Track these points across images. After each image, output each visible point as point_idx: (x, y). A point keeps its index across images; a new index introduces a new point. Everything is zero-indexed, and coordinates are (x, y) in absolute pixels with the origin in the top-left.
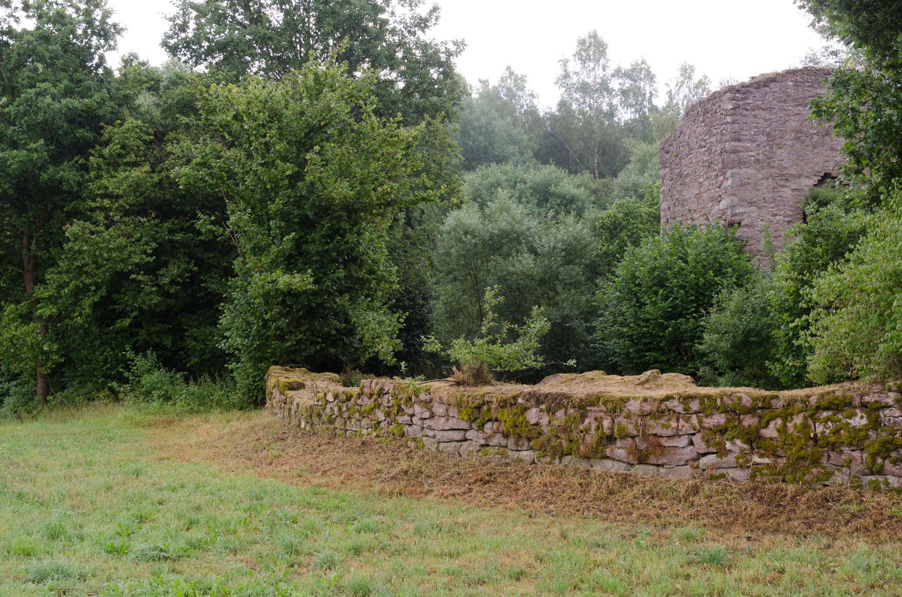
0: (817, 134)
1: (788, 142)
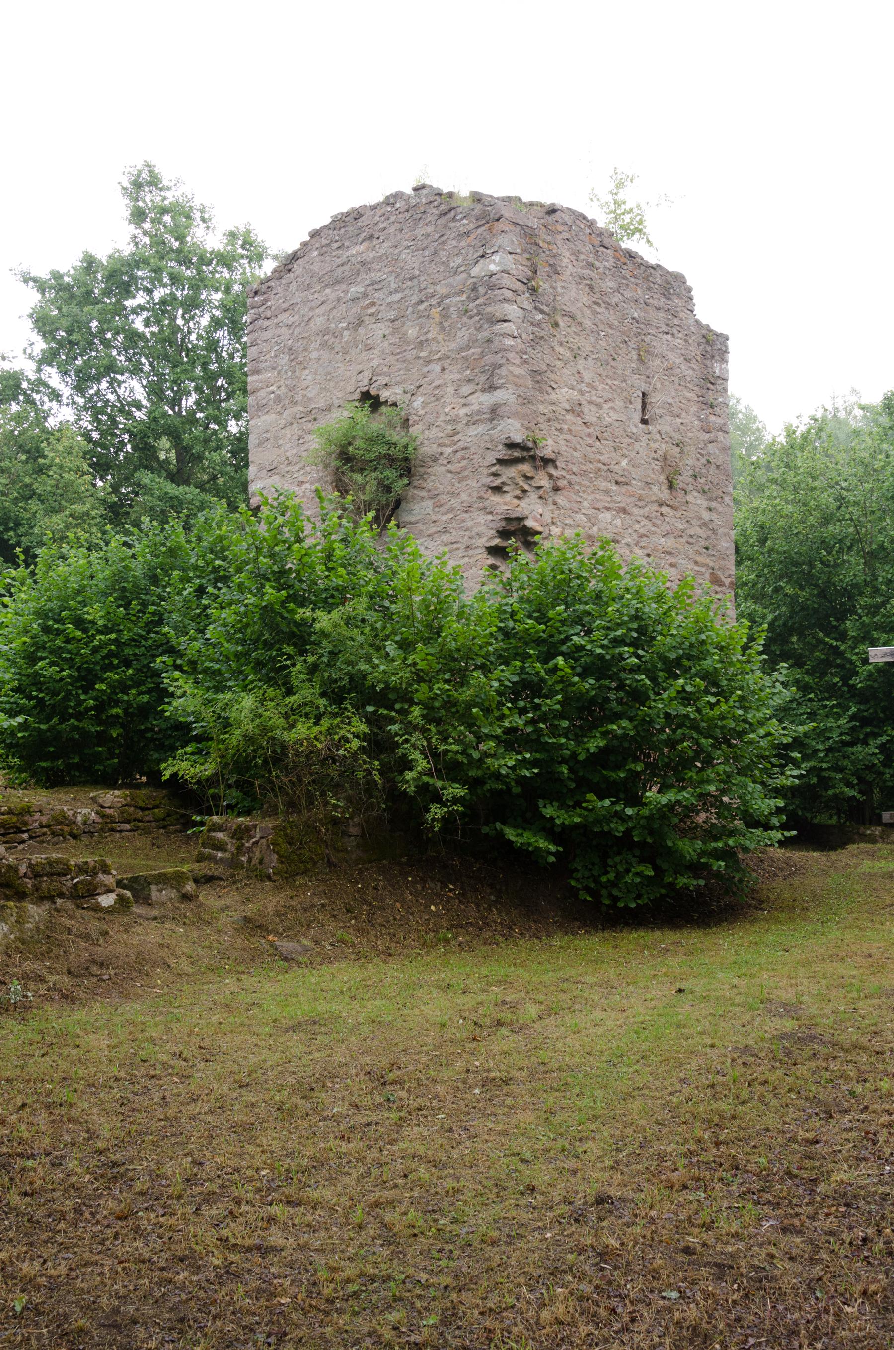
0: (347, 329)
1: (315, 355)
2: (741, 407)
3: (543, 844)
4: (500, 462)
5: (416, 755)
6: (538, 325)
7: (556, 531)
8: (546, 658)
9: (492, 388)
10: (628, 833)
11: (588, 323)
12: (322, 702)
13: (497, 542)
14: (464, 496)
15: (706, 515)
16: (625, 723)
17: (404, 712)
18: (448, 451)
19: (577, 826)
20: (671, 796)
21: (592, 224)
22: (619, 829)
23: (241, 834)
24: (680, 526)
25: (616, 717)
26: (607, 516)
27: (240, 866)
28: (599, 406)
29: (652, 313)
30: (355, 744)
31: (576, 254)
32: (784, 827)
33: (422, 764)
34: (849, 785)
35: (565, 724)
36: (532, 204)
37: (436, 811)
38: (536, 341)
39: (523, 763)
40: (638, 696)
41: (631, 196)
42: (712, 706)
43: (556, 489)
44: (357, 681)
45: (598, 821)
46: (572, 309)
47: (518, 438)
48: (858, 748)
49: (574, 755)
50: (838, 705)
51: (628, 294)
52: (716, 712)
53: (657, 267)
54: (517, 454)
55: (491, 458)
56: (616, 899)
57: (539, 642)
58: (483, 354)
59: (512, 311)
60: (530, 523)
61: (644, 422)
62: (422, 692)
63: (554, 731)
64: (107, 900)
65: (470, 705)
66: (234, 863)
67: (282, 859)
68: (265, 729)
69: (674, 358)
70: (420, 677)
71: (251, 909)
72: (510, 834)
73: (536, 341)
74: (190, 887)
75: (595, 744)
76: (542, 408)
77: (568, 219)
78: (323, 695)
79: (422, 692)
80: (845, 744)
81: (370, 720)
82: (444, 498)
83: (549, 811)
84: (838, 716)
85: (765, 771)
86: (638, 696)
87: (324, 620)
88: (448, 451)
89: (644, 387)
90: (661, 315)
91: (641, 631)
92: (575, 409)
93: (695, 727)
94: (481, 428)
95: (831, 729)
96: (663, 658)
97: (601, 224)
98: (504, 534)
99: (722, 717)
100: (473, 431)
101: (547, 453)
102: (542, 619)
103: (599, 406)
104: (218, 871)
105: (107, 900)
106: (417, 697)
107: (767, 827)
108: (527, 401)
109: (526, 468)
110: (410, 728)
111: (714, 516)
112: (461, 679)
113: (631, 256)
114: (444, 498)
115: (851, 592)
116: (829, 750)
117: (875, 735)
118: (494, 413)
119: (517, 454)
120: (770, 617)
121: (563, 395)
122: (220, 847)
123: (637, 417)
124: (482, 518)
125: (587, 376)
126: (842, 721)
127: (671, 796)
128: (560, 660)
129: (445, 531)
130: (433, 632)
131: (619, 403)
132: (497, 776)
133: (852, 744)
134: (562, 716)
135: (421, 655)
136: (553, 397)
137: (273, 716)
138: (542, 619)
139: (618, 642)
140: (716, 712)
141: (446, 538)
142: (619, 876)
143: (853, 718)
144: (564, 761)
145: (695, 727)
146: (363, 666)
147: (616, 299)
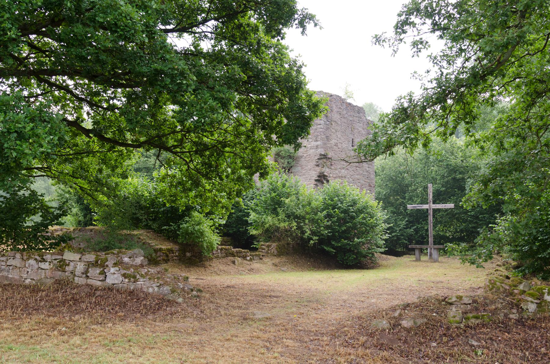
2: (379, 109)
3: (332, 250)
4: (318, 159)
5: (307, 230)
6: (328, 125)
7: (331, 175)
8: (333, 209)
9: (317, 141)
10: (350, 248)
11: (339, 123)
12: (286, 218)
13: (317, 178)
14: (309, 167)
15: (368, 169)
16: (350, 224)
17: (304, 221)
18: (305, 155)
19: (340, 246)
20: (360, 240)
21: (340, 97)
22: (348, 247)
23: (268, 246)
24: (361, 172)
25: (348, 222)
26: (343, 171)
27: (268, 253)
28: (342, 143)
29: (355, 118)
30: (295, 228)
31: (337, 106)
32: (385, 248)
33: (309, 232)
34: (406, 240)
35: (337, 224)
36: (326, 93)
37: (312, 242)
38: (328, 129)
39: (328, 232)
40: (353, 218)
41: (350, 89)
42: (369, 220)
43: (331, 165)
44: (293, 213)
45: (344, 245)
46: (336, 120)
47: (323, 153)
48: (408, 230)
49: (339, 231)
50: (403, 218)
51: (349, 114)
52: (370, 222)
53: (356, 106)
54: (322, 157)
55: (317, 158)
56: (347, 263)
57: (331, 205)
58: (314, 132)
59: (322, 122)
60: (325, 174)
61: (353, 146)
62: (308, 216)
63: (335, 225)
64: (248, 258)
65: (318, 220)
66: (267, 253)
67: (278, 252)
68: (274, 224)
69: (360, 129)
70: (307, 213)
71: (273, 262)
72: (325, 248)
73: (328, 129)
74: (261, 257)
75: (344, 228)
76: (328, 145)
77: (335, 97)
78: (286, 217)
79: (308, 216)
80: (404, 228)
81: (297, 222)
82: (304, 166)
83: (333, 243)
84: (403, 220)
85: (381, 235)
86: (353, 218)
87: (287, 201)
88: (305, 155)
89: (353, 137)
90: (357, 118)
91: (354, 203)
92: (336, 145)
93: (365, 225)
94: (314, 150)
95: (401, 224)
96: (359, 209)
97: (343, 97)
98: (319, 176)
99: (372, 223)
100: (312, 151)
101: (329, 156)
102: (332, 200)
103: (342, 143)
104: (264, 254)
105: (248, 258)
106: (307, 218)
107: (381, 248)
108: (325, 144)
109: (325, 160)
110: (305, 224)
111: (370, 169)
112: (316, 214)
113: (350, 104)
114: (304, 166)
115: (407, 186)
116: (400, 230)
117: (413, 226)
118: (317, 147)
119: (322, 157)
120: (384, 193)
121: (333, 142)
122: (264, 249)
123: (351, 145)
124: (314, 172)
125: (339, 136)
126: (404, 222)
127: (360, 240)
128: (336, 210)
129: (304, 175)
130: (310, 204)
131: (347, 142)
132: (323, 235)
133: (406, 228)
134: (336, 222)
135: (308, 209)
136: (331, 142)
137: (277, 222)
138: (332, 200)
139: (349, 206)
140: (370, 222)
141: (304, 176)
142: (348, 258)
143: (407, 221)
144: (337, 232)
145: (365, 225)
146: (295, 211)
147: (346, 116)
